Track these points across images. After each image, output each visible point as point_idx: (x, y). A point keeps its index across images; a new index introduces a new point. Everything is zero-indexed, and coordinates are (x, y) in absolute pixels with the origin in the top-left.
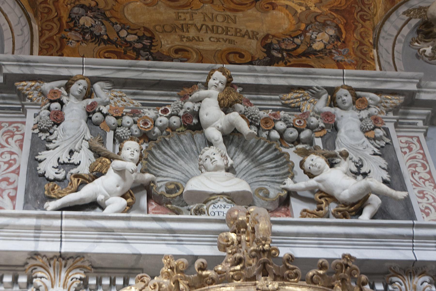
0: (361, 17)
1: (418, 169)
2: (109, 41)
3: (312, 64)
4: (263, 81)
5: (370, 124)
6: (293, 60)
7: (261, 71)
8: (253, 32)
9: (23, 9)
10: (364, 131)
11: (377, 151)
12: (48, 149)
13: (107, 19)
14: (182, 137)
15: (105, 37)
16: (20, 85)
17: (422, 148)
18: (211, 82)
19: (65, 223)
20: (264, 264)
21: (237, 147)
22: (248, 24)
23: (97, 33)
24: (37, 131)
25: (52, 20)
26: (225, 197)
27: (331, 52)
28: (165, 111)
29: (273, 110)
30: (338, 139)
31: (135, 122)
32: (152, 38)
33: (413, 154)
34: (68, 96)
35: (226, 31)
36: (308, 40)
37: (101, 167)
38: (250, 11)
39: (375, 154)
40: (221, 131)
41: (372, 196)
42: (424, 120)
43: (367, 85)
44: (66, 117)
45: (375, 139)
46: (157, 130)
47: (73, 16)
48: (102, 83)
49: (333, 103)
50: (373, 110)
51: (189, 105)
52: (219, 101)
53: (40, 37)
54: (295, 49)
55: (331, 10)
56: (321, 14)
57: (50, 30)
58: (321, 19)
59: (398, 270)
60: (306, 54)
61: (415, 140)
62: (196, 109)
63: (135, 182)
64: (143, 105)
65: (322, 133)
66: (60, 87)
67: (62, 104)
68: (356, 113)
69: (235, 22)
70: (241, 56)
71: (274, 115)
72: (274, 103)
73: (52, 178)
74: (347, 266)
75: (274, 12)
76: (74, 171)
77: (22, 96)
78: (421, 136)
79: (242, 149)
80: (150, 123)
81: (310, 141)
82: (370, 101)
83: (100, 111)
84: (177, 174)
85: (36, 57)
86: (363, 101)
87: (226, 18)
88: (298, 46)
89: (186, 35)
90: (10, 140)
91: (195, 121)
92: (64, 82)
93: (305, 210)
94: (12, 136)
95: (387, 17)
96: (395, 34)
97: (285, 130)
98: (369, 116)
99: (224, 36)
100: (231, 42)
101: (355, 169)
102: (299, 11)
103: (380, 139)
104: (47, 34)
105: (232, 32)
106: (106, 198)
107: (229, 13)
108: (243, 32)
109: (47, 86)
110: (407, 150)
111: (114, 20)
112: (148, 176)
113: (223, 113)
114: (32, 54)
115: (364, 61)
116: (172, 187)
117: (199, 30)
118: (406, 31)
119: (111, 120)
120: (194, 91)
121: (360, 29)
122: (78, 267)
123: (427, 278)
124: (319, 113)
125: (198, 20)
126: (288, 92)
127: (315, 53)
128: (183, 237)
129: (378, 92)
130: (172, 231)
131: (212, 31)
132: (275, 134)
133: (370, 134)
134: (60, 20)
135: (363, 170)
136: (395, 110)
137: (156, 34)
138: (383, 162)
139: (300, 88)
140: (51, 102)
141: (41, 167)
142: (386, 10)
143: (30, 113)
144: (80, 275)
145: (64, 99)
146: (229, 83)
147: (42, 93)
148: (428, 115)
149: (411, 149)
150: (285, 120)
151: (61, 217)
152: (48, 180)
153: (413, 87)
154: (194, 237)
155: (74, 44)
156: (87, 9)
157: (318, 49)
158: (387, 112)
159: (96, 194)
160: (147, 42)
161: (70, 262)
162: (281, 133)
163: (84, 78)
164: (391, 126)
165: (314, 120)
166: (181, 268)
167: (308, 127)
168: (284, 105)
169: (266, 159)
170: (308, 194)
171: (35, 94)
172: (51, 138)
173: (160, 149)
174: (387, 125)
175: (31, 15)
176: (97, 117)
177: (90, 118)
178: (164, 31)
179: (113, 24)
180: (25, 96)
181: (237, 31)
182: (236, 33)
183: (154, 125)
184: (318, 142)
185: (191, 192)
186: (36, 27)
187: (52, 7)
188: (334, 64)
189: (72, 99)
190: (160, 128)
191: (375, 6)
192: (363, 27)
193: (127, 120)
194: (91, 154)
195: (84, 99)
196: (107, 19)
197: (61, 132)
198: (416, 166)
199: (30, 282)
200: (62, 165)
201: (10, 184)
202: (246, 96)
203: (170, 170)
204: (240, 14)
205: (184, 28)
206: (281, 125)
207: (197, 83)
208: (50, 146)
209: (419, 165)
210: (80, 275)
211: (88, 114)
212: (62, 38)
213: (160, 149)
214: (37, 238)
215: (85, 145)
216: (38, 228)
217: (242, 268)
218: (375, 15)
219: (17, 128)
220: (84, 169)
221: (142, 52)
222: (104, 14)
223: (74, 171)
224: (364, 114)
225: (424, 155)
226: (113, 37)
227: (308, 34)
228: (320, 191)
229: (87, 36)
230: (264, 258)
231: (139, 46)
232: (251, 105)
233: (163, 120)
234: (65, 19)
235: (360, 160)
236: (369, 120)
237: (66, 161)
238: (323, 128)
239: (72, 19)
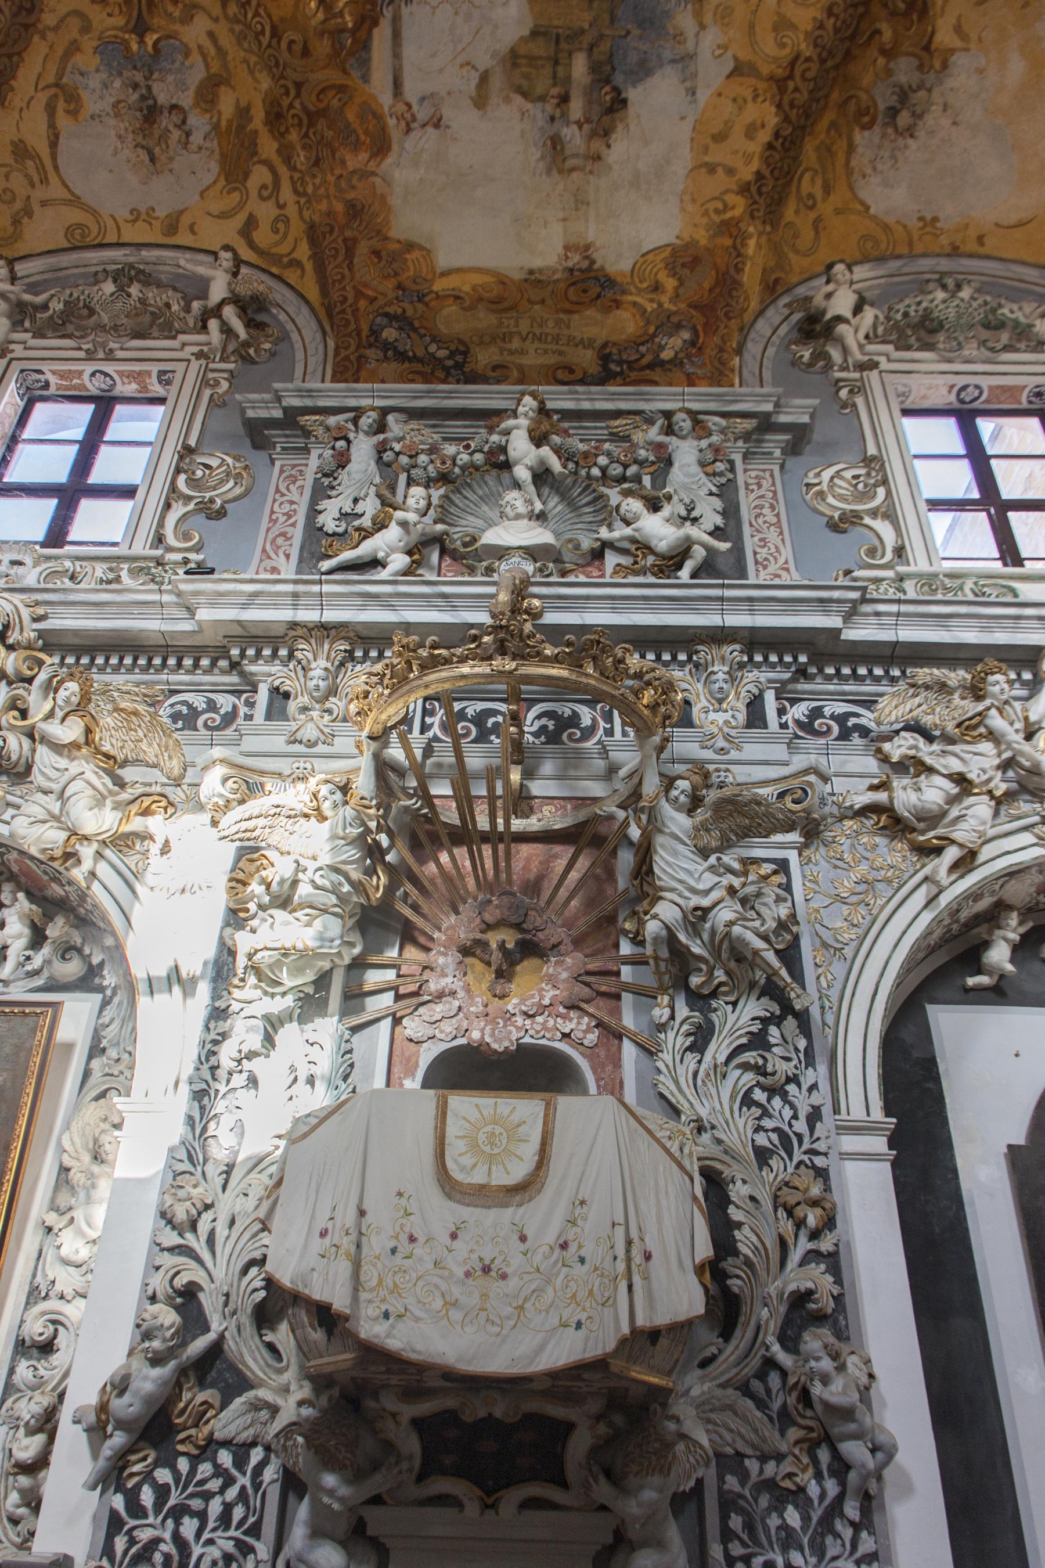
0: (726, 315)
1: (764, 511)
2: (415, 359)
3: (657, 379)
4: (586, 405)
5: (709, 456)
6: (634, 375)
7: (584, 393)
8: (589, 339)
9: (320, 322)
10: (702, 464)
11: (714, 489)
12: (330, 497)
13: (415, 330)
14: (487, 478)
15: (411, 354)
16: (306, 420)
17: (773, 484)
18: (521, 409)
19: (326, 588)
20: (502, 641)
21: (552, 488)
22: (585, 329)
23: (401, 348)
24: (319, 475)
25: (350, 335)
26: (521, 552)
27: (682, 363)
28: (467, 447)
29: (597, 441)
30: (670, 476)
31: (432, 462)
32: (466, 353)
33: (761, 492)
34: (357, 431)
35: (556, 339)
36: (655, 347)
37: (384, 519)
38: (588, 313)
39: (711, 494)
40: (531, 469)
41: (696, 547)
42: (782, 449)
43: (712, 406)
44: (353, 458)
45: (714, 474)
46: (457, 470)
47: (375, 328)
48: (396, 414)
49: (669, 430)
50: (715, 439)
51: (495, 438)
52: (530, 431)
53: (335, 356)
54: (637, 360)
55: (690, 306)
56: (675, 313)
57: (346, 348)
58: (675, 319)
59: (704, 637)
60: (651, 366)
61: (768, 474)
62: (503, 443)
63: (423, 534)
64: (445, 439)
65: (652, 469)
66: (346, 421)
67: (349, 442)
68: (695, 443)
69: (568, 328)
70: (572, 371)
71: (596, 448)
72: (599, 432)
73: (330, 532)
74: (598, 642)
75: (618, 312)
76: (356, 523)
77: (307, 433)
78: (776, 469)
79: (558, 492)
80: (449, 462)
81: (637, 479)
82: (713, 428)
83: (392, 449)
84: (479, 523)
85: (328, 385)
86: (704, 428)
87: (558, 323)
88: (643, 356)
89: (508, 346)
90: (291, 487)
91: (502, 458)
92: (352, 415)
93: (618, 565)
94: (294, 482)
95: (761, 313)
96: (769, 334)
97: (607, 467)
98: (710, 445)
99: (554, 347)
100: (561, 353)
101: (684, 513)
102: (649, 309)
103: (721, 474)
104: (343, 353)
105: (564, 341)
106: (388, 555)
107: (562, 316)
108: (578, 340)
109: (332, 421)
110: (755, 487)
111: (422, 331)
112: (440, 527)
113: (533, 448)
114: (323, 381)
115: (721, 373)
116: (468, 539)
117: (524, 340)
118: (783, 330)
119: (404, 460)
120: (502, 421)
121: (722, 331)
122: (343, 638)
123: (737, 647)
124: (650, 443)
125: (524, 326)
126: (616, 419)
127: (662, 364)
128: (457, 602)
129: (724, 415)
130: (444, 596)
131: (540, 340)
132: (596, 472)
133: (709, 469)
134: (359, 334)
135: (694, 514)
136: (746, 436)
137: (471, 346)
138: (717, 503)
139: (630, 413)
140: (337, 439)
141: (321, 519)
142: (762, 302)
143: (314, 453)
144: (345, 646)
145: (351, 436)
146: (543, 411)
147: (328, 429)
148: (787, 442)
149: (760, 486)
150: (609, 454)
151: (320, 582)
152: (327, 534)
153: (768, 407)
154: (469, 602)
155: (373, 365)
156: (391, 317)
157: (667, 358)
158: (736, 440)
159: (376, 551)
160: (459, 358)
161: (333, 632)
162: (604, 470)
163: (373, 409)
164: (737, 458)
165: (642, 453)
166: (411, 646)
167: (636, 462)
168: (611, 434)
169: (584, 502)
170: (626, 545)
171: (321, 430)
172: (335, 483)
173: (460, 493)
174: (733, 456)
175: (328, 328)
176: (388, 456)
177: (381, 458)
178: (482, 343)
179: (422, 336)
180: (310, 432)
181: (570, 339)
182: (569, 341)
183: (454, 464)
184: (647, 481)
185: (486, 546)
186: (331, 344)
187: (350, 317)
188: (684, 378)
189: (361, 436)
190: (461, 467)
191: (747, 299)
192: (726, 327)
193: (423, 458)
194: (378, 502)
195: (375, 434)
196: (415, 330)
197: (346, 477)
198: (762, 507)
199: (291, 656)
200: (344, 516)
201: (288, 539)
202: (566, 425)
203: (471, 518)
204: (576, 317)
205: (506, 337)
206: (602, 460)
207: (506, 410)
208: (333, 493)
209: (767, 505)
210: (345, 646)
211: (379, 452)
212: (360, 357)
213: (460, 493)
214: (295, 607)
215: (373, 489)
216: (295, 595)
217: (477, 647)
218: (745, 310)
219: (301, 471)
220: (366, 522)
221: (452, 371)
222: (411, 324)
223: (356, 523)
224: (704, 444)
225: (775, 492)
226: (420, 352)
227: (657, 340)
228: (638, 542)
229: (390, 353)
230: (502, 635)
231: (450, 363)
232: (569, 436)
233: (464, 458)
234: (365, 333)
235: (692, 501)
236: (708, 452)
237: (349, 511)
238: (653, 463)
239: (375, 332)
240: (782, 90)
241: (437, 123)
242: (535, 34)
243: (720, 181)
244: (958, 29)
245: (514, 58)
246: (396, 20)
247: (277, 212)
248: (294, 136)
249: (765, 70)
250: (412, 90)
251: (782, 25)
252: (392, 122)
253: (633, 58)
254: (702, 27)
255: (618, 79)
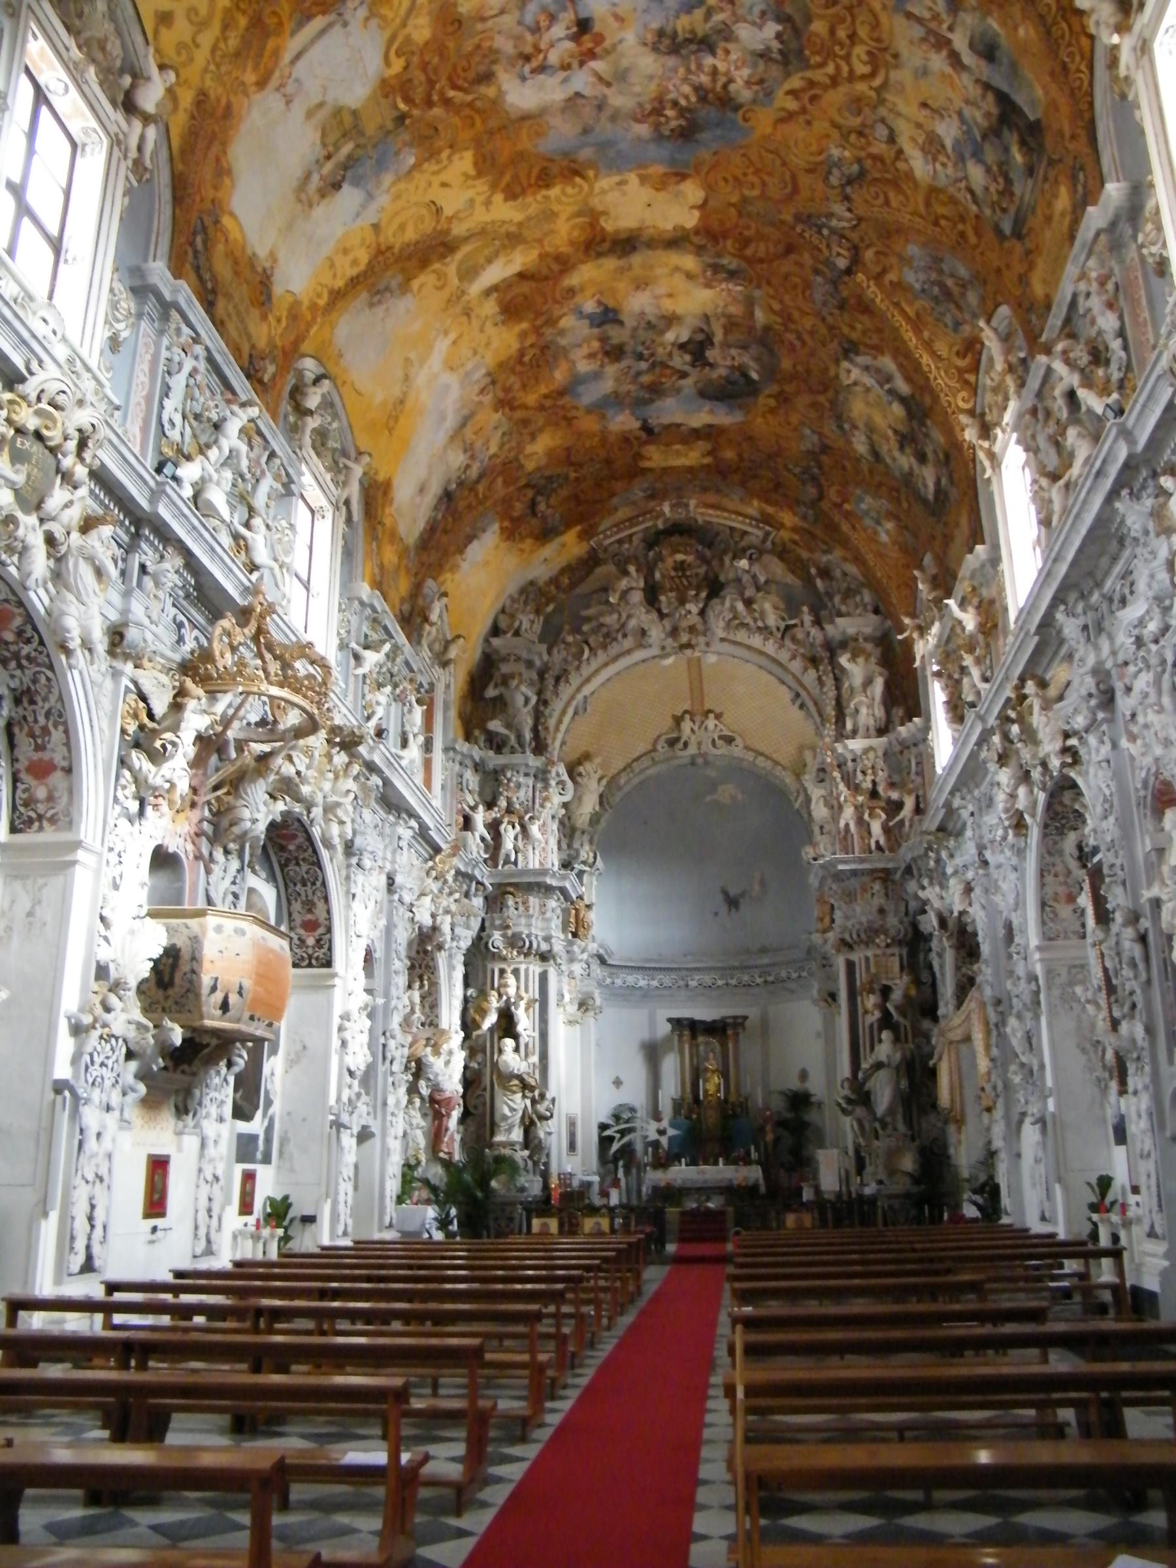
16: (174, 314)
240: (376, 256)
241: (288, 103)
242: (355, 113)
243: (327, 279)
244: (422, 286)
245: (338, 112)
246: (330, 25)
247: (188, 40)
248: (243, 22)
249: (382, 239)
250: (300, 69)
251: (402, 227)
252: (277, 74)
253: (361, 171)
254: (388, 191)
255: (349, 174)
